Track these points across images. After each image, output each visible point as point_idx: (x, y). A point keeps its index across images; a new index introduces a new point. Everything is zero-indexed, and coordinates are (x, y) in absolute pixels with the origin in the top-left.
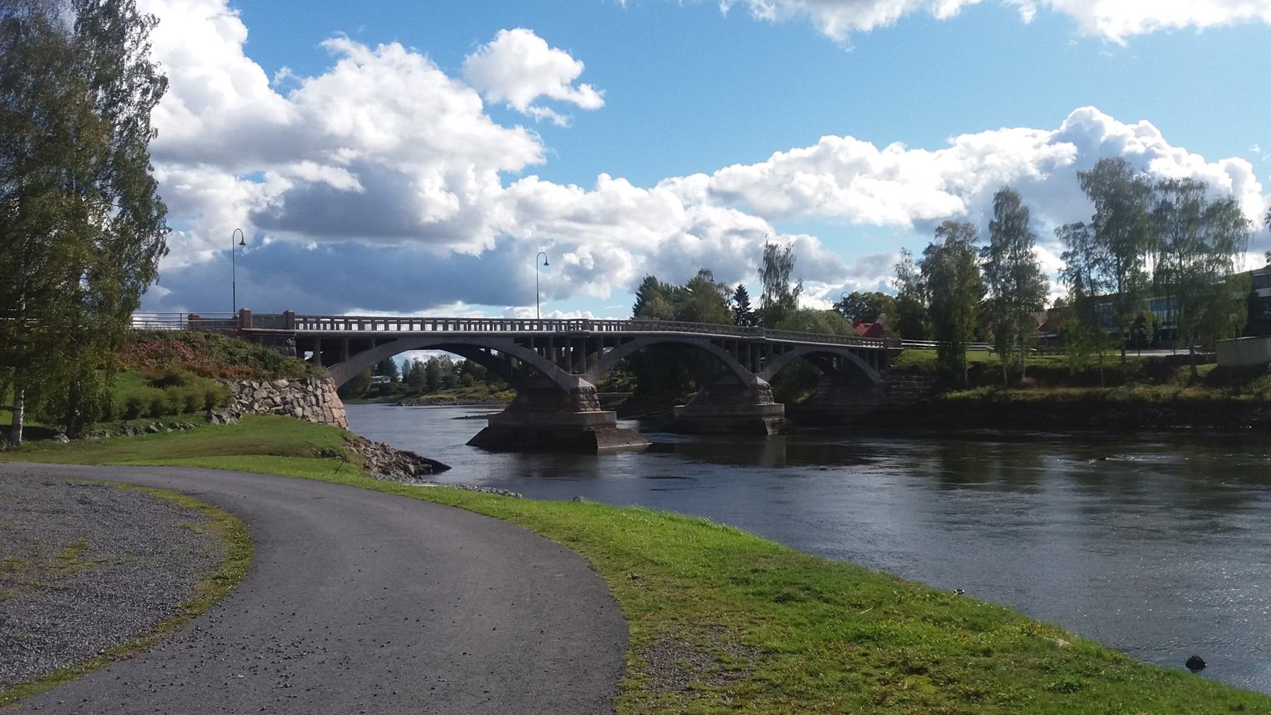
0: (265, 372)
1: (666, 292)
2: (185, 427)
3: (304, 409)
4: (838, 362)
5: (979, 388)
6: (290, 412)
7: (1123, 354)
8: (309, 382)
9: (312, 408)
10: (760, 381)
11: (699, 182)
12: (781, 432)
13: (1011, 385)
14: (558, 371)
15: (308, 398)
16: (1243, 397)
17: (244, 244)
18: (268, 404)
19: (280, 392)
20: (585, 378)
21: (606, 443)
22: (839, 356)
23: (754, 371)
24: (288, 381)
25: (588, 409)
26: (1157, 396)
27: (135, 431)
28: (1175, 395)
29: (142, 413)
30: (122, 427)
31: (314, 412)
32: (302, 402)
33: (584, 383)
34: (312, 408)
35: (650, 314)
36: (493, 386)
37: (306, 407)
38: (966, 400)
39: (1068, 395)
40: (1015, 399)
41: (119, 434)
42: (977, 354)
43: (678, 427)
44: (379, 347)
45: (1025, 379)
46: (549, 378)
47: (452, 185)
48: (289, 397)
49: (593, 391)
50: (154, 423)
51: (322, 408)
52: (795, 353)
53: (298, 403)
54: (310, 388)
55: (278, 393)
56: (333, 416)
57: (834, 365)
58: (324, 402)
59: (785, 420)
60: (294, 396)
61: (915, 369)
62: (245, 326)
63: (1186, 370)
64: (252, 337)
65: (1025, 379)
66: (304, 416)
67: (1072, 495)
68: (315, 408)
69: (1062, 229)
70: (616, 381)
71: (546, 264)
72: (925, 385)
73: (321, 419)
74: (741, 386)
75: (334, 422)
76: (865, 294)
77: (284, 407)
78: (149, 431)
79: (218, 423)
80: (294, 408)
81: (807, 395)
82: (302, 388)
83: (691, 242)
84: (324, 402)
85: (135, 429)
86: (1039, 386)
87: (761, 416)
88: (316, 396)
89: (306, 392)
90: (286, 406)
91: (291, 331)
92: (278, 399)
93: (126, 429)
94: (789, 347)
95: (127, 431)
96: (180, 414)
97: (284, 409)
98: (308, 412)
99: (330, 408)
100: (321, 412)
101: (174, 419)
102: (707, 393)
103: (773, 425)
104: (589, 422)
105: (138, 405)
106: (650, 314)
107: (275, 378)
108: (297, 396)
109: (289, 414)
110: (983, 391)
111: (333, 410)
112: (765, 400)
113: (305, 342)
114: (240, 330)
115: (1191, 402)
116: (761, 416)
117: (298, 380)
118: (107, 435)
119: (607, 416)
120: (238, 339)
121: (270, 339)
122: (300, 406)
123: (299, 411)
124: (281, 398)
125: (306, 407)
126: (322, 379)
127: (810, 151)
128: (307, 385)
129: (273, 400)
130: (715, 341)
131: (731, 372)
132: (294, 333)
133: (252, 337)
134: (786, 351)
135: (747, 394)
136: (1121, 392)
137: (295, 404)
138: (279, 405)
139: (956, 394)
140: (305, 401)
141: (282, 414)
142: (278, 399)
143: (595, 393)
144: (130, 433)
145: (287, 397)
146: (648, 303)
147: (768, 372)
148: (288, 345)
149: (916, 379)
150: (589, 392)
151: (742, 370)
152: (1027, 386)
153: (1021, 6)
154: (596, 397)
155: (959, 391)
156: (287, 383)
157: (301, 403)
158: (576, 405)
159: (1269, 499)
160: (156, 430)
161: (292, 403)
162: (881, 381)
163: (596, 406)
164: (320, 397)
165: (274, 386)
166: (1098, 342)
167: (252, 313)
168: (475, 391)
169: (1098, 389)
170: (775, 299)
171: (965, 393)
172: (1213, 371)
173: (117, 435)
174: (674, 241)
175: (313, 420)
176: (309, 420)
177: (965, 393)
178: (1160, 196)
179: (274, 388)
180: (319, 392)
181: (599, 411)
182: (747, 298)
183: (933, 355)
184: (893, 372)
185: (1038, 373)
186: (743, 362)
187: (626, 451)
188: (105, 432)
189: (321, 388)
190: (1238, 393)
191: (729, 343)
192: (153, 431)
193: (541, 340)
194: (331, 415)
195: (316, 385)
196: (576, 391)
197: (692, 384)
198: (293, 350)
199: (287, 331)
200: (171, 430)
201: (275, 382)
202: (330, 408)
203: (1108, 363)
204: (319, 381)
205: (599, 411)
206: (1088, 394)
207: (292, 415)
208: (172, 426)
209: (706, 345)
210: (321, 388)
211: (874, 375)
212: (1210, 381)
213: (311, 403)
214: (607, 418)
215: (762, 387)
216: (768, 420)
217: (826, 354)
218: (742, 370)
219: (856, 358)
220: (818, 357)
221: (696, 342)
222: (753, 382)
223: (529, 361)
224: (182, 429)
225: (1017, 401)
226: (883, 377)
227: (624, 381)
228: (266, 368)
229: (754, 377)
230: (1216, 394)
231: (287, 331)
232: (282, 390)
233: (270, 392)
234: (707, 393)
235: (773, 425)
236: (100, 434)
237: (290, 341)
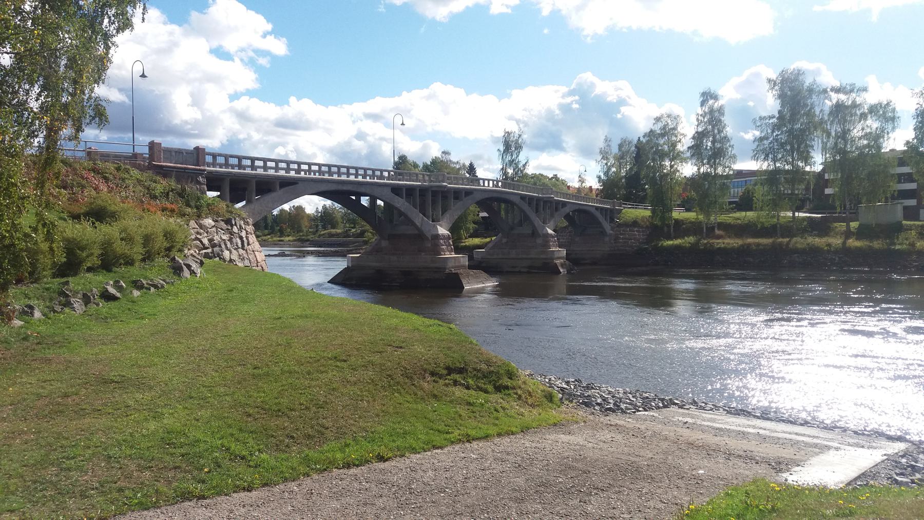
0: (189, 210)
2: (156, 287)
3: (231, 252)
5: (686, 238)
6: (219, 255)
7: (794, 214)
8: (234, 223)
9: (238, 252)
11: (359, 108)
13: (708, 236)
14: (423, 220)
15: (234, 240)
16: (898, 247)
17: (146, 77)
18: (197, 247)
19: (207, 233)
20: (441, 226)
21: (469, 283)
24: (213, 221)
25: (446, 253)
26: (829, 245)
27: (87, 300)
28: (773, 242)
29: (89, 265)
30: (62, 294)
31: (240, 255)
32: (228, 244)
33: (442, 231)
34: (238, 252)
37: (233, 250)
39: (758, 245)
40: (718, 246)
41: (58, 308)
44: (282, 190)
45: (717, 232)
47: (196, 101)
48: (217, 239)
49: (449, 238)
50: (111, 282)
51: (246, 251)
53: (226, 245)
54: (235, 229)
55: (206, 235)
56: (257, 260)
58: (248, 244)
60: (221, 238)
61: (635, 223)
62: (155, 160)
64: (164, 172)
65: (717, 232)
66: (231, 261)
67: (897, 328)
68: (241, 251)
69: (758, 119)
70: (350, 230)
71: (403, 124)
72: (643, 235)
73: (247, 263)
74: (534, 234)
75: (258, 266)
76: (532, 174)
77: (213, 250)
78: (107, 297)
79: (189, 276)
80: (222, 251)
82: (228, 229)
83: (358, 144)
84: (248, 244)
85: (85, 295)
86: (729, 237)
88: (241, 238)
89: (231, 233)
90: (215, 249)
91: (202, 168)
92: (206, 241)
93: (67, 296)
95: (72, 300)
96: (137, 264)
97: (213, 252)
98: (235, 256)
99: (253, 251)
100: (245, 256)
101: (135, 271)
102: (504, 240)
103: (562, 265)
105: (83, 251)
107: (199, 216)
108: (224, 237)
109: (218, 258)
110: (691, 239)
111: (256, 253)
113: (214, 182)
114: (150, 163)
115: (859, 250)
117: (223, 220)
118: (37, 314)
119: (462, 259)
120: (150, 173)
121: (182, 175)
122: (227, 249)
123: (226, 254)
124: (209, 240)
125: (233, 250)
126: (243, 219)
127: (425, 92)
128: (232, 226)
129: (201, 242)
130: (523, 197)
132: (205, 170)
133: (164, 172)
134: (562, 208)
135: (539, 241)
136: (799, 242)
137: (223, 246)
138: (207, 248)
140: (231, 244)
141: (210, 258)
142: (206, 241)
143: (450, 239)
144: (78, 304)
145: (215, 238)
148: (199, 183)
149: (637, 231)
152: (719, 237)
153: (289, 105)
156: (213, 223)
157: (228, 246)
158: (436, 250)
160: (118, 295)
161: (220, 246)
162: (611, 232)
164: (245, 239)
165: (201, 226)
166: (776, 203)
167: (162, 146)
170: (510, 171)
171: (678, 242)
173: (55, 311)
174: (348, 143)
175: (240, 265)
176: (236, 264)
178: (835, 97)
179: (201, 228)
180: (243, 234)
184: (620, 225)
185: (729, 229)
188: (31, 308)
189: (245, 230)
192: (112, 298)
194: (255, 259)
195: (240, 226)
196: (437, 237)
198: (204, 188)
199: (197, 167)
200: (139, 293)
201: (201, 222)
202: (253, 251)
203: (782, 221)
204: (243, 222)
207: (220, 258)
208: (137, 285)
210: (245, 230)
211: (607, 226)
213: (237, 246)
214: (462, 261)
220: (582, 212)
222: (544, 232)
223: (402, 210)
224: (152, 289)
225: (719, 248)
226: (612, 229)
227: (356, 231)
228: (188, 205)
229: (544, 228)
231: (197, 167)
232: (209, 230)
233: (198, 233)
234: (504, 240)
235: (562, 265)
236: (24, 313)
237: (201, 179)
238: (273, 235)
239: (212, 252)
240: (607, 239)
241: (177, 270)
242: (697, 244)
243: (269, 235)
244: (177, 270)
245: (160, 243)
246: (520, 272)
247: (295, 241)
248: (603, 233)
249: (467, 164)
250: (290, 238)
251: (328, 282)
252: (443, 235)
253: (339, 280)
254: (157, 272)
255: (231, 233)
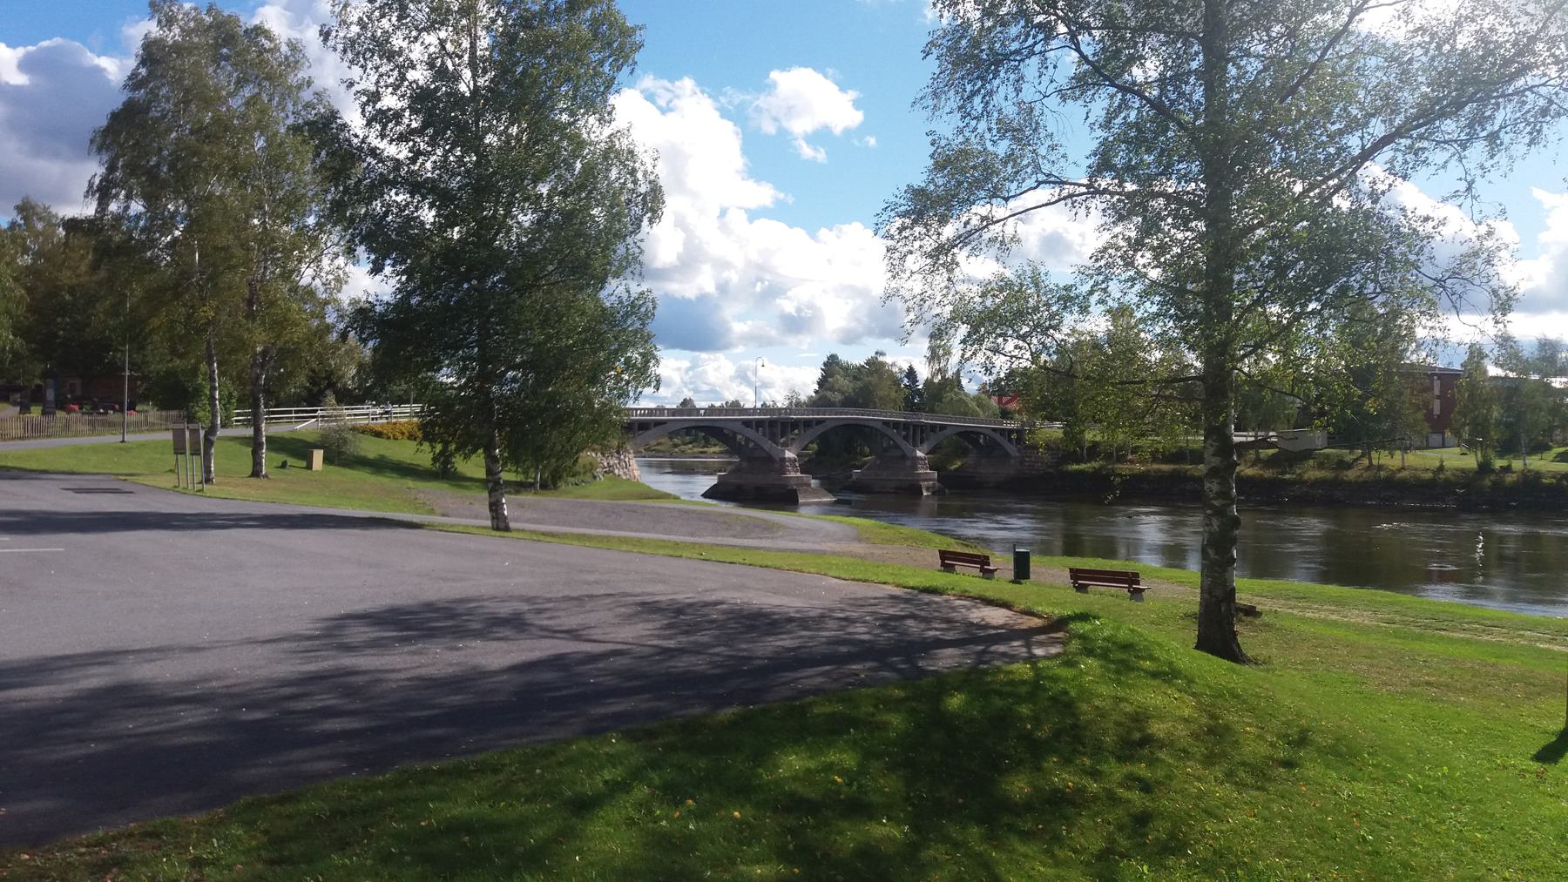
1: (846, 369)
4: (985, 438)
10: (919, 454)
12: (934, 493)
16: (1287, 476)
20: (789, 450)
22: (985, 435)
23: (915, 445)
33: (789, 454)
35: (832, 389)
36: (676, 440)
38: (1082, 472)
39: (1160, 470)
42: (1091, 435)
43: (857, 488)
46: (764, 451)
48: (611, 463)
52: (947, 432)
57: (981, 441)
59: (937, 484)
63: (1251, 455)
74: (904, 457)
81: (959, 463)
87: (918, 481)
89: (619, 459)
94: (943, 427)
98: (621, 473)
101: (582, 477)
104: (792, 482)
106: (832, 389)
110: (1095, 464)
112: (923, 468)
116: (918, 481)
123: (616, 471)
130: (885, 423)
131: (897, 447)
135: (908, 463)
139: (1075, 467)
146: (830, 379)
147: (926, 446)
150: (792, 461)
151: (906, 446)
154: (797, 464)
155: (1077, 464)
158: (783, 470)
159: (1567, 599)
163: (797, 471)
168: (658, 444)
169: (1182, 466)
171: (1082, 466)
172: (1273, 455)
177: (1082, 466)
181: (799, 474)
182: (916, 377)
183: (1060, 434)
186: (906, 438)
187: (372, 647)
190: (1284, 473)
191: (896, 425)
193: (760, 423)
196: (783, 460)
197: (867, 450)
205: (799, 474)
206: (1174, 470)
209: (879, 426)
211: (1012, 450)
212: (1270, 462)
215: (920, 458)
216: (924, 484)
217: (973, 432)
218: (906, 446)
219: (997, 437)
221: (871, 424)
226: (1019, 451)
230: (1268, 474)
235: (928, 489)
238: (695, 444)
239: (609, 471)
240: (1012, 461)
241: (595, 477)
242: (1102, 467)
243: (690, 443)
244: (595, 477)
245: (589, 467)
246: (888, 492)
247: (721, 453)
248: (1007, 455)
249: (905, 367)
250: (717, 449)
251: (705, 495)
252: (789, 459)
253: (711, 494)
254: (588, 477)
255: (619, 459)
